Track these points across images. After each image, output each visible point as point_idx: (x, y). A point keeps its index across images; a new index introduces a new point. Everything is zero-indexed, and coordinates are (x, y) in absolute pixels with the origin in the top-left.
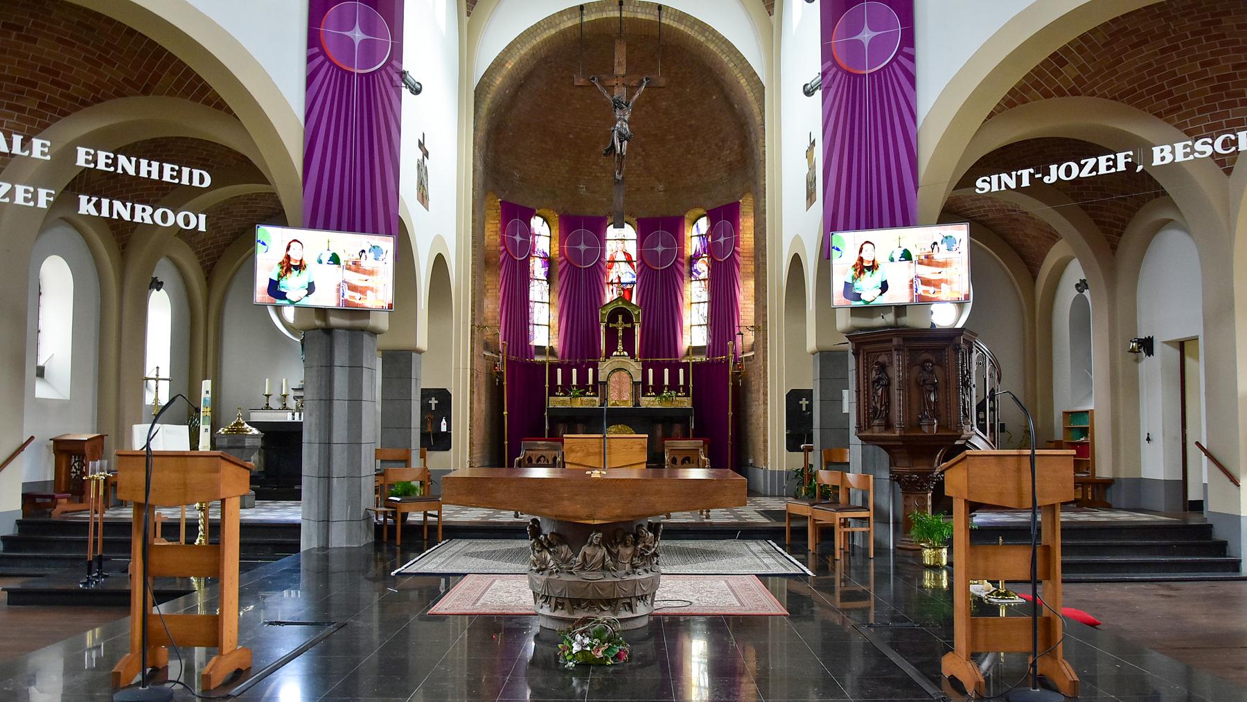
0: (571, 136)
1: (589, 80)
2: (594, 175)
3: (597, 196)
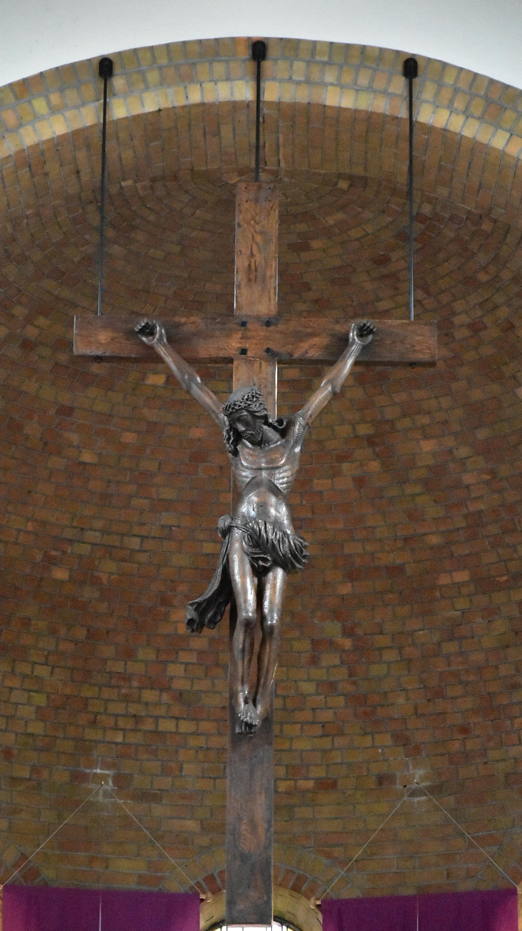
0: (61, 574)
1: (131, 334)
2: (148, 726)
3: (158, 810)
